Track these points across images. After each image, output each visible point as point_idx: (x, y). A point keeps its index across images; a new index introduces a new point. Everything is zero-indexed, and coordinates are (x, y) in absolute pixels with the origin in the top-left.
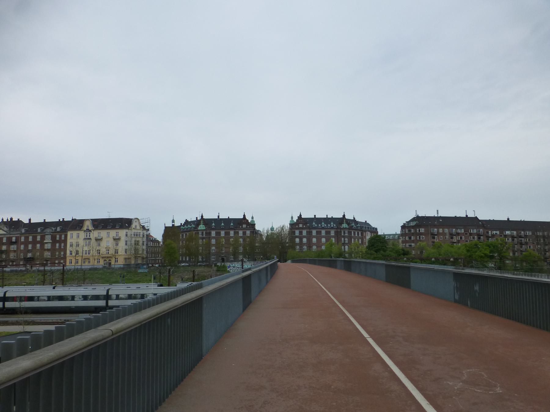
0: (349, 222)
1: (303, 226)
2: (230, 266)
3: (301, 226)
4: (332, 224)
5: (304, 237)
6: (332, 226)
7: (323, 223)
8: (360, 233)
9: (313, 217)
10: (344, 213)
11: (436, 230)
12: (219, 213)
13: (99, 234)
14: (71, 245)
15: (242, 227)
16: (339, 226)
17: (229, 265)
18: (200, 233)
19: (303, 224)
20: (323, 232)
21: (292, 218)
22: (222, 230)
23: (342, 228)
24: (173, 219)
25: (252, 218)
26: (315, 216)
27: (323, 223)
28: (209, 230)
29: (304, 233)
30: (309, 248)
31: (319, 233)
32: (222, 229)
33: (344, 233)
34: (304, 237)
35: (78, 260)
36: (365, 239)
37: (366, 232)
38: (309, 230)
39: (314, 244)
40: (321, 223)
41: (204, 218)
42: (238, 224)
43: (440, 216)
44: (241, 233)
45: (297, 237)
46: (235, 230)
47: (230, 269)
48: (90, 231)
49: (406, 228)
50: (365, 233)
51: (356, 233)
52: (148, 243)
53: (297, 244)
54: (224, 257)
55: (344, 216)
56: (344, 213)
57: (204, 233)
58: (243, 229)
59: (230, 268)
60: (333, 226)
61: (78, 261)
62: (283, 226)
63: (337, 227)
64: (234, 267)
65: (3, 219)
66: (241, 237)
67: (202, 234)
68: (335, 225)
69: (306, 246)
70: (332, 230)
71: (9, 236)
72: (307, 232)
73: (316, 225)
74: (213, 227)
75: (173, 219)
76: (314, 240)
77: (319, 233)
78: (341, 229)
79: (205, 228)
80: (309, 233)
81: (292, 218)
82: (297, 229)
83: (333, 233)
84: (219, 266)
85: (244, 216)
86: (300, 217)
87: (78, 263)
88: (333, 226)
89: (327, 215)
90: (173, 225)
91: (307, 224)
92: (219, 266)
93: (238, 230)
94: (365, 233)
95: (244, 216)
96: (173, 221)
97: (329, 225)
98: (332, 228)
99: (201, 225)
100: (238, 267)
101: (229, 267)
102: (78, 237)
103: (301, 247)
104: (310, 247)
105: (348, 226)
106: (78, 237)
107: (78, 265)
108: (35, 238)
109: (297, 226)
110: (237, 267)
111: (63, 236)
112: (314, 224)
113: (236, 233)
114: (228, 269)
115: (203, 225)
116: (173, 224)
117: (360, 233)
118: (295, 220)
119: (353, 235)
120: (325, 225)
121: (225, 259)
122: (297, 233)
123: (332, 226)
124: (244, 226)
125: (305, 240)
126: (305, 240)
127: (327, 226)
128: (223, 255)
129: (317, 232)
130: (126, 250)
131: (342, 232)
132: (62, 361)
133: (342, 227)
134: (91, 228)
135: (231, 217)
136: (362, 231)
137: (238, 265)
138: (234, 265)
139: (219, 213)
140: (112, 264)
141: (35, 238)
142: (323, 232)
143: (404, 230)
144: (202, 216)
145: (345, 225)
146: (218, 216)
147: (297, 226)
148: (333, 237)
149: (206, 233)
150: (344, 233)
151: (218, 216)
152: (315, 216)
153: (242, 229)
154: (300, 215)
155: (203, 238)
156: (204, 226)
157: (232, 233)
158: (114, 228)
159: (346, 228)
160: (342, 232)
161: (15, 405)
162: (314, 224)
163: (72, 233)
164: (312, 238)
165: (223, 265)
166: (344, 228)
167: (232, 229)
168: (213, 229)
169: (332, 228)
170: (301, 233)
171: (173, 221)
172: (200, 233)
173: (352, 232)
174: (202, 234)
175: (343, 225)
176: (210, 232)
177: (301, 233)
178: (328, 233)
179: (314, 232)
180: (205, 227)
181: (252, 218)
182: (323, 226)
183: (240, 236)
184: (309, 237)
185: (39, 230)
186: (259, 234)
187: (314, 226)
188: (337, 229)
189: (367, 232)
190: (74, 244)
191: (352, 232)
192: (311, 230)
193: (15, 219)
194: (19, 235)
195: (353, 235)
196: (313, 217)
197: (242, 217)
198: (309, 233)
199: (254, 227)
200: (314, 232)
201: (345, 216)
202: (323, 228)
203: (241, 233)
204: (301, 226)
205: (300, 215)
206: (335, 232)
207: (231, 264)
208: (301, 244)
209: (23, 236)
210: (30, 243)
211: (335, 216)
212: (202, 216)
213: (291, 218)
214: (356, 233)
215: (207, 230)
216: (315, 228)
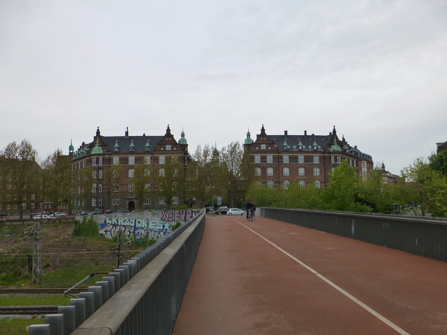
1: (267, 147)
2: (105, 222)
3: (263, 147)
4: (315, 144)
6: (315, 148)
7: (300, 144)
8: (355, 161)
9: (283, 134)
10: (98, 127)
12: (127, 128)
15: (164, 150)
16: (326, 149)
17: (103, 221)
18: (94, 160)
19: (268, 144)
20: (301, 159)
21: (249, 135)
22: (131, 155)
23: (332, 152)
24: (71, 145)
25: (183, 135)
26: (286, 132)
27: (300, 144)
28: (108, 154)
29: (270, 159)
30: (277, 184)
31: (294, 159)
32: (132, 153)
33: (336, 160)
34: (270, 165)
37: (361, 161)
38: (278, 155)
39: (287, 178)
40: (297, 144)
41: (101, 134)
42: (158, 144)
44: (162, 159)
45: (258, 166)
46: (152, 154)
47: (106, 231)
48: (274, 201)
52: (339, 205)
53: (257, 178)
54: (134, 200)
57: (101, 159)
58: (165, 154)
59: (105, 229)
60: (317, 148)
62: (235, 145)
63: (325, 150)
64: (115, 225)
66: (162, 166)
67: (97, 162)
68: (319, 147)
69: (273, 180)
70: (315, 155)
72: (274, 157)
73: (289, 147)
74: (116, 150)
75: (71, 145)
76: (286, 171)
77: (294, 159)
78: (330, 153)
79: (101, 152)
80: (278, 160)
81: (249, 135)
82: (257, 152)
83: (316, 160)
84: (81, 222)
85: (168, 130)
86: (263, 135)
88: (317, 148)
91: (274, 144)
92: (81, 222)
93: (157, 154)
95: (168, 130)
98: (316, 151)
100: (125, 226)
101: (104, 225)
104: (279, 183)
105: (341, 148)
109: (257, 148)
110: (124, 226)
112: (285, 144)
113: (155, 160)
114: (102, 231)
115: (99, 146)
116: (71, 151)
117: (355, 161)
118: (254, 138)
120: (304, 147)
121: (136, 203)
122: (257, 159)
123: (315, 148)
124: (168, 147)
125: (270, 171)
126: (270, 171)
128: (132, 196)
129: (290, 158)
131: (333, 159)
133: (332, 150)
135: (149, 133)
136: (357, 158)
137: (124, 221)
138: (114, 220)
139: (127, 128)
142: (301, 159)
145: (336, 148)
146: (127, 133)
147: (257, 148)
148: (316, 165)
149: (103, 160)
150: (336, 160)
151: (127, 133)
152: (286, 132)
153: (165, 152)
154: (263, 130)
155: (99, 169)
156: (100, 147)
157: (148, 158)
159: (338, 152)
160: (333, 159)
161: (88, 287)
162: (285, 144)
164: (283, 168)
165: (90, 221)
166: (335, 152)
167: (147, 153)
168: (116, 153)
169: (316, 151)
170: (264, 159)
172: (94, 160)
174: (97, 162)
175: (333, 146)
176: (109, 157)
177: (264, 159)
178: (308, 159)
179: (286, 159)
180: (103, 149)
181: (183, 135)
182: (300, 148)
184: (277, 167)
186: (197, 166)
187: (285, 148)
188: (322, 153)
189: (362, 161)
192: (280, 155)
196: (283, 134)
198: (278, 160)
199: (185, 149)
200: (286, 159)
202: (301, 152)
203: (162, 159)
204: (263, 147)
206: (320, 158)
207: (107, 219)
208: (264, 178)
211: (317, 133)
213: (247, 136)
215: (106, 155)
216: (287, 151)
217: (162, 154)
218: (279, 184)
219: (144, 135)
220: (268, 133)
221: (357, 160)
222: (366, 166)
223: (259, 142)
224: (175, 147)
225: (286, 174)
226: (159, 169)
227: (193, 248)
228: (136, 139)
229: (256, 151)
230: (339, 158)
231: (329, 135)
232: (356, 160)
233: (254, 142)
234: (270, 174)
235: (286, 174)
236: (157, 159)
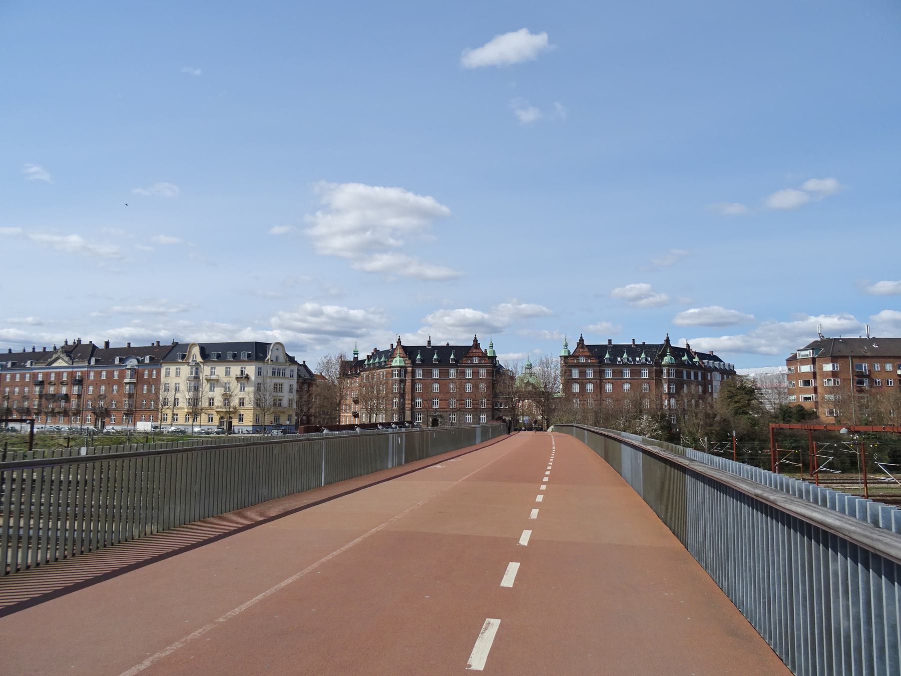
0: (678, 352)
3: (582, 360)
5: (590, 381)
8: (700, 374)
10: (668, 335)
11: (865, 367)
13: (213, 370)
14: (167, 390)
26: (610, 341)
35: (167, 415)
36: (709, 386)
43: (874, 338)
44: (469, 373)
49: (798, 364)
50: (709, 374)
51: (692, 373)
55: (668, 340)
56: (668, 335)
60: (646, 360)
61: (168, 416)
65: (66, 342)
71: (70, 370)
82: (575, 366)
87: (212, 421)
88: (646, 360)
89: (634, 340)
90: (356, 359)
94: (709, 374)
95: (475, 340)
96: (356, 353)
97: (638, 359)
99: (398, 359)
102: (178, 374)
103: (584, 401)
106: (178, 374)
107: (178, 423)
108: (110, 375)
111: (154, 372)
116: (356, 356)
117: (700, 374)
119: (685, 377)
126: (590, 387)
127: (634, 360)
130: (290, 400)
132: (818, 526)
134: (199, 359)
140: (233, 424)
141: (110, 375)
143: (793, 368)
144: (399, 342)
146: (429, 342)
151: (429, 342)
152: (610, 341)
154: (582, 340)
158: (236, 358)
163: (179, 367)
164: (586, 383)
171: (356, 353)
173: (685, 373)
183: (467, 379)
184: (598, 381)
185: (117, 361)
190: (172, 386)
191: (685, 373)
193: (85, 341)
194: (86, 369)
195: (685, 377)
197: (471, 344)
201: (669, 340)
203: (469, 373)
205: (582, 340)
209: (105, 370)
210: (103, 382)
212: (399, 342)
214: (692, 373)
217: (469, 367)
218: (370, 421)
219: (10, 350)
220: (13, 352)
221: (703, 371)
222: (718, 379)
223: (577, 354)
224: (154, 369)
225: (609, 390)
226: (466, 383)
227: (734, 432)
228: (440, 349)
229: (573, 364)
230: (645, 372)
231: (445, 346)
232: (701, 373)
233: (571, 354)
234: (590, 390)
235: (609, 390)
236: (464, 373)
